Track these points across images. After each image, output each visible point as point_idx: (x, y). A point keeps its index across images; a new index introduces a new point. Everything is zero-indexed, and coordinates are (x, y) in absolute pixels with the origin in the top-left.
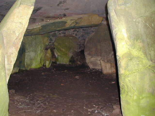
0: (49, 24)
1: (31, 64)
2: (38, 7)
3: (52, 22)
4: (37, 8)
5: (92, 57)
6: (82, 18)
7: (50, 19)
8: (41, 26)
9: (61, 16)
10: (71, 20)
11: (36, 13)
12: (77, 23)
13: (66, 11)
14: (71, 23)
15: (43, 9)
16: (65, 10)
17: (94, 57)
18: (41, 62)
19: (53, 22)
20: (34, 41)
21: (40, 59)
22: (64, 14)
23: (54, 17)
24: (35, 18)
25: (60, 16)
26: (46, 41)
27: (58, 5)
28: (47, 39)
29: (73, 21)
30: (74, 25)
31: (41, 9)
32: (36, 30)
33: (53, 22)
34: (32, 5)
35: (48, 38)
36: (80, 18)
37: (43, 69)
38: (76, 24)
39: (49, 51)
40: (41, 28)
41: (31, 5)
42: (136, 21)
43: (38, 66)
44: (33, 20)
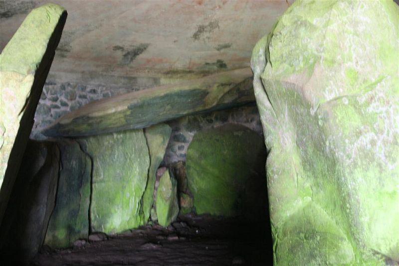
0: (155, 98)
1: (105, 217)
2: (135, 44)
3: (162, 94)
4: (135, 48)
7: (179, 75)
8: (128, 108)
9: (211, 67)
10: (222, 85)
11: (134, 60)
14: (222, 94)
15: (150, 49)
18: (141, 212)
19: (165, 95)
20: (120, 147)
21: (138, 200)
22: (219, 61)
23: (190, 72)
24: (133, 76)
25: (208, 67)
26: (158, 144)
27: (196, 36)
28: (162, 139)
29: (227, 89)
30: (234, 98)
31: (145, 49)
32: (114, 118)
33: (165, 93)
34: (29, 72)
35: (164, 138)
37: (148, 234)
38: (239, 97)
40: (129, 113)
41: (25, 71)
42: (316, 113)
43: (133, 223)
44: (126, 80)
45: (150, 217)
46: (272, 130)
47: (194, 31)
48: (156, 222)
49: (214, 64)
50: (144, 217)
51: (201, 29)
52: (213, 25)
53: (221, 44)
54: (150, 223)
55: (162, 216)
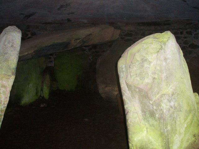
5: (106, 87)
6: (91, 34)
10: (76, 39)
12: (84, 42)
13: (70, 15)
16: (68, 14)
17: (109, 87)
18: (37, 93)
22: (68, 19)
27: (59, 9)
29: (78, 41)
36: (89, 35)
38: (83, 44)
39: (48, 77)
45: (41, 95)
46: (129, 103)
47: (58, 7)
48: (43, 97)
49: (66, 20)
50: (38, 95)
51: (62, 6)
52: (68, 5)
53: (70, 12)
54: (41, 98)
55: (46, 93)
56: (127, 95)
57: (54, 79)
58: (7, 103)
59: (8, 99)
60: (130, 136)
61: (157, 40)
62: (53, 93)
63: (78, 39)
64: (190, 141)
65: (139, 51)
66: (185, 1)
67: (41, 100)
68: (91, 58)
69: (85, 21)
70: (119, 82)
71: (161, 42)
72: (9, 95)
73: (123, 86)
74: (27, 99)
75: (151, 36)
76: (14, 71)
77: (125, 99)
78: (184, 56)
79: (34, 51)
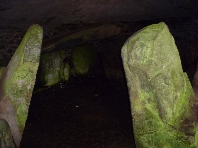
27: (73, 13)
39: (67, 64)
48: (65, 80)
56: (129, 73)
57: (72, 66)
58: (34, 84)
59: (34, 81)
60: (132, 108)
61: (153, 29)
62: (71, 76)
63: (88, 35)
64: (181, 112)
65: (138, 39)
66: (172, 2)
67: (62, 81)
68: (99, 49)
69: (94, 22)
70: (124, 72)
71: (156, 31)
72: (35, 78)
73: (126, 68)
74: (51, 80)
75: (149, 27)
76: (38, 58)
77: (128, 78)
78: (176, 43)
79: (56, 46)
